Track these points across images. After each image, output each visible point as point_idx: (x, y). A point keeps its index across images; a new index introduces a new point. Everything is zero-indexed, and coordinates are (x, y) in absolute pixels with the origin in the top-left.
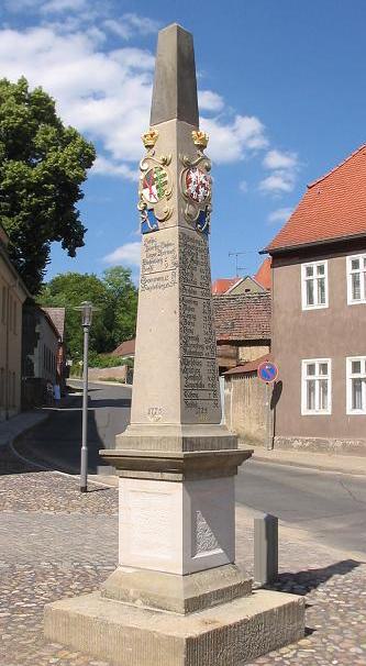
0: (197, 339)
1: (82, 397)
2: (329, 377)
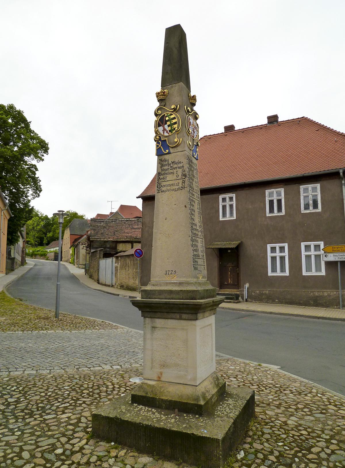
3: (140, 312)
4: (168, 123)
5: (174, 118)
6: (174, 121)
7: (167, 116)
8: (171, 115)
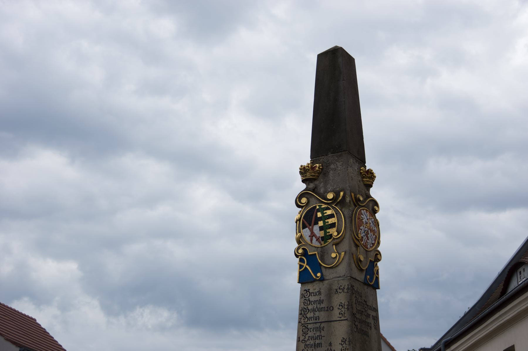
4: (321, 223)
5: (331, 216)
6: (331, 221)
7: (318, 210)
8: (328, 209)
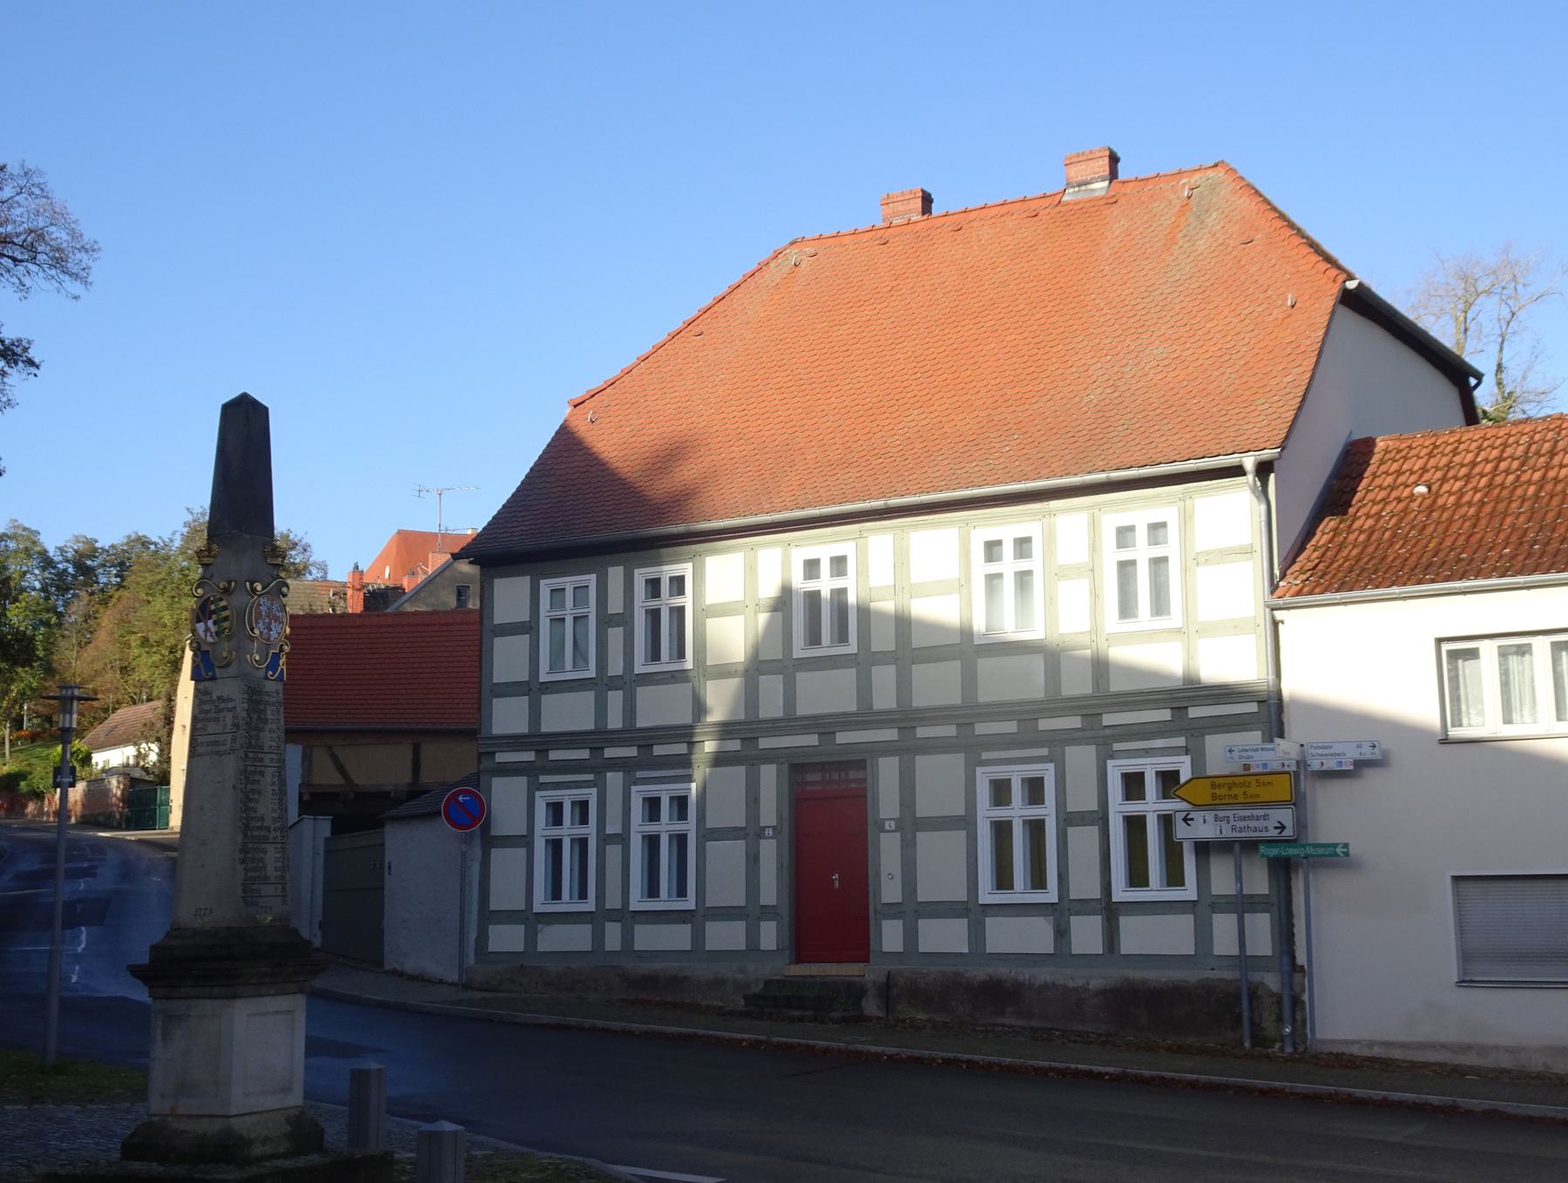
0: (262, 819)
1: (67, 861)
2: (590, 831)
3: (147, 988)
5: (225, 608)
6: (225, 614)
7: (212, 603)
